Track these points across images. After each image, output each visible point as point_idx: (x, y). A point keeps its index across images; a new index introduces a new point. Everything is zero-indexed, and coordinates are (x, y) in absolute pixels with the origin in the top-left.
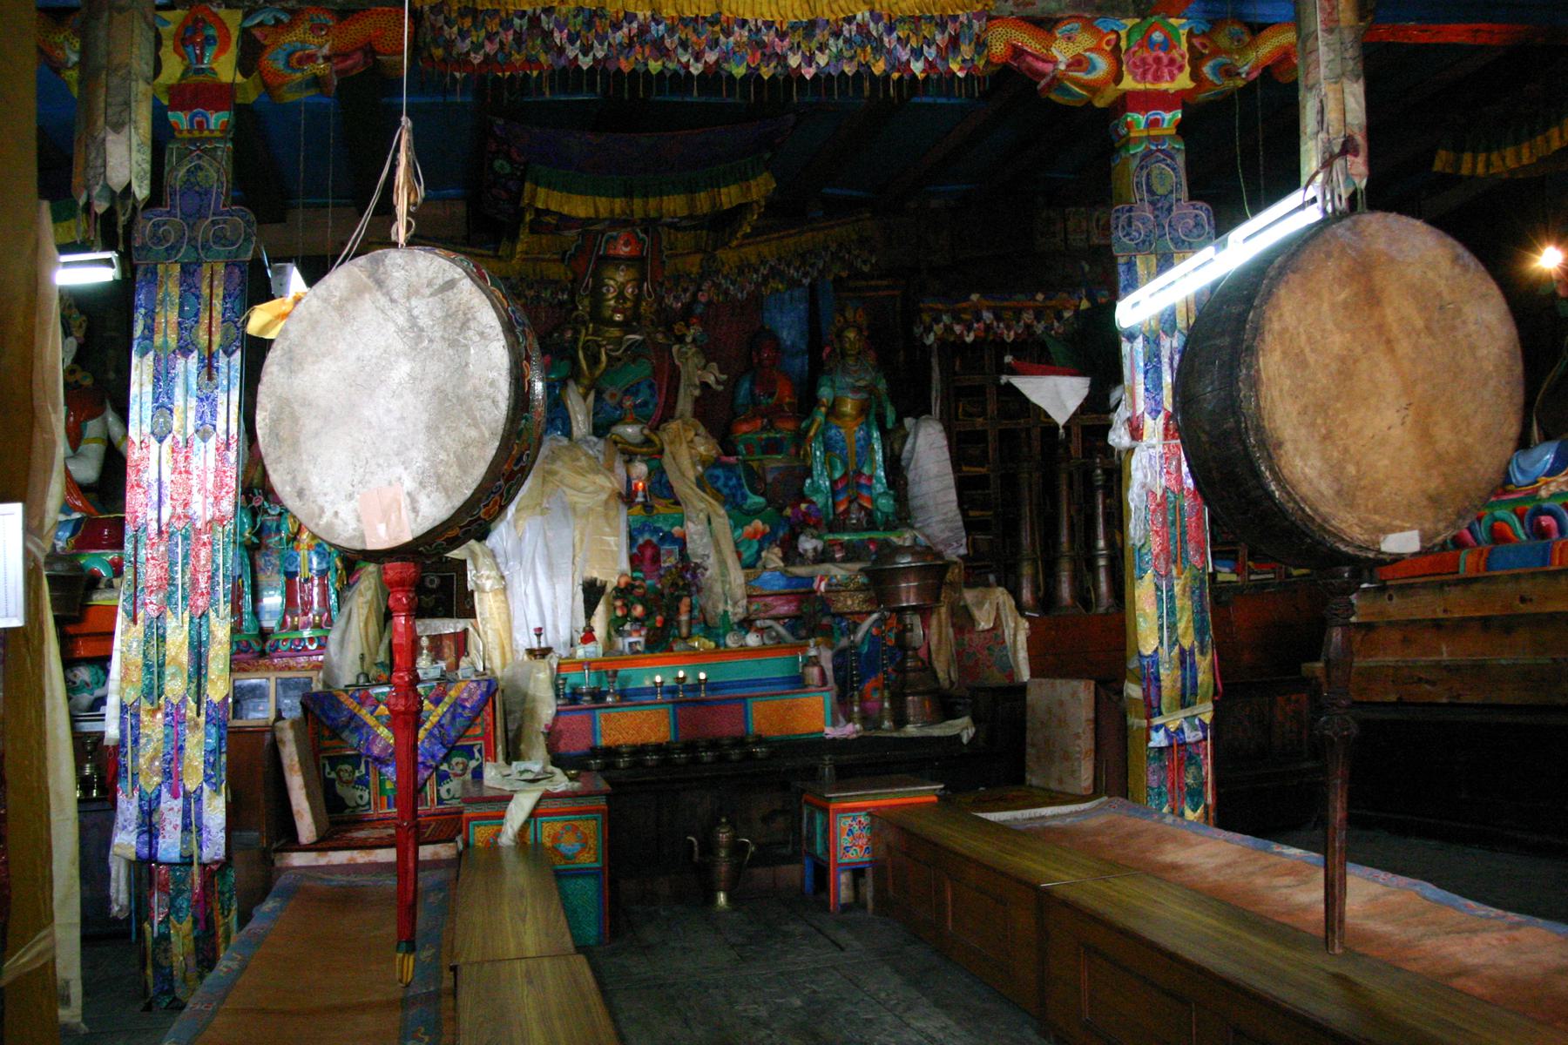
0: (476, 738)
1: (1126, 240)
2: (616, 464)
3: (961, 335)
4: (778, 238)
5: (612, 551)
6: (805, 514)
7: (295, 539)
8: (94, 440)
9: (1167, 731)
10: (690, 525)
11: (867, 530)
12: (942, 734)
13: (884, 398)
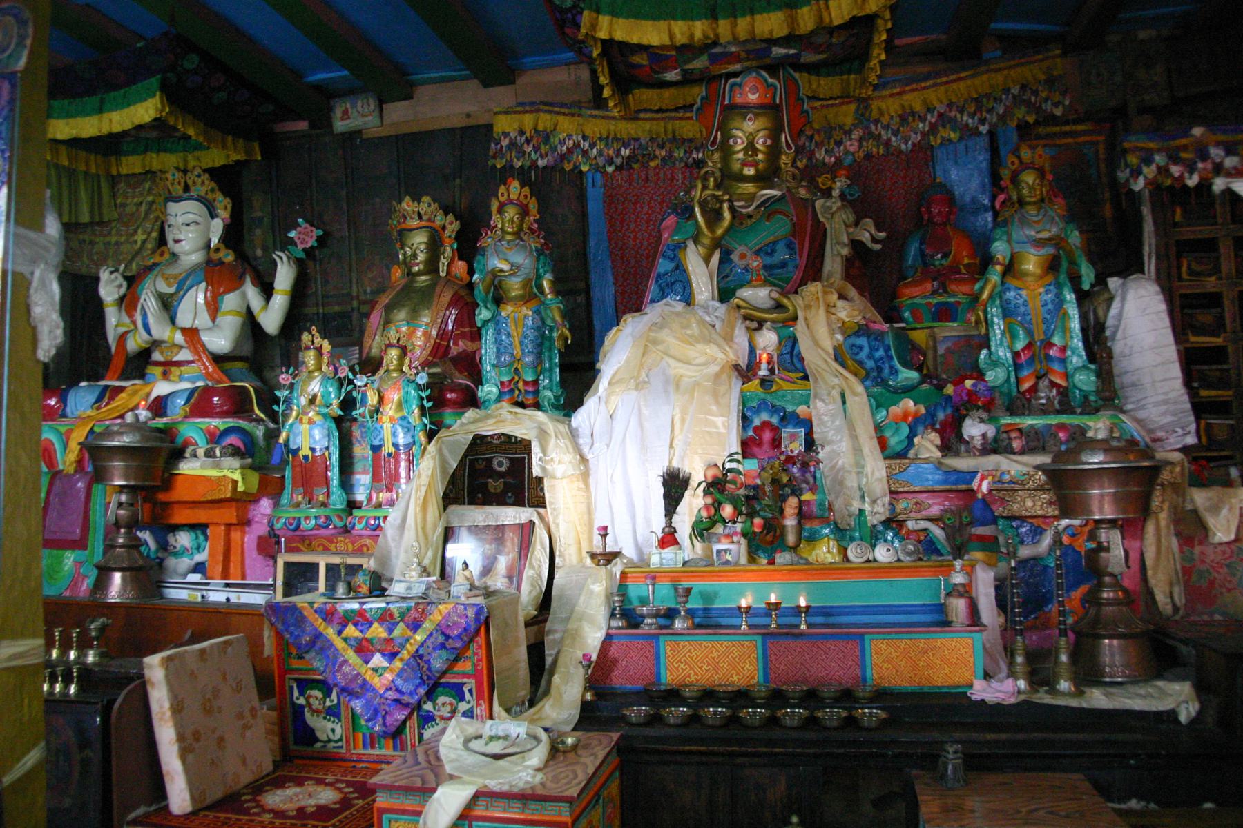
0: (468, 676)
2: (737, 332)
3: (1182, 176)
4: (947, 83)
5: (719, 434)
6: (970, 393)
7: (377, 411)
8: (230, 312)
10: (819, 404)
11: (1058, 412)
12: (1146, 708)
13: (1078, 253)
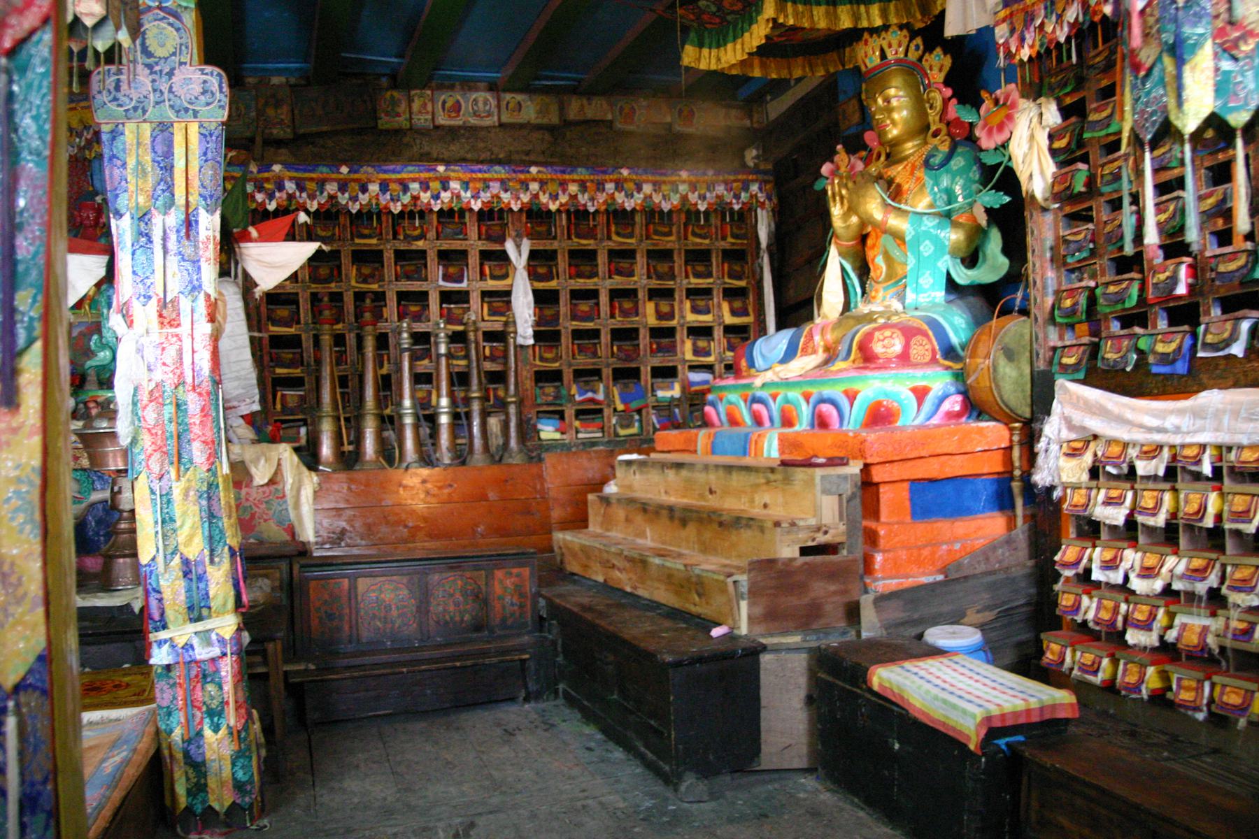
1: (113, 106)
3: (263, 203)
9: (173, 646)
